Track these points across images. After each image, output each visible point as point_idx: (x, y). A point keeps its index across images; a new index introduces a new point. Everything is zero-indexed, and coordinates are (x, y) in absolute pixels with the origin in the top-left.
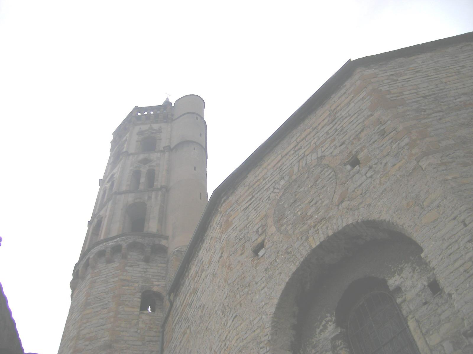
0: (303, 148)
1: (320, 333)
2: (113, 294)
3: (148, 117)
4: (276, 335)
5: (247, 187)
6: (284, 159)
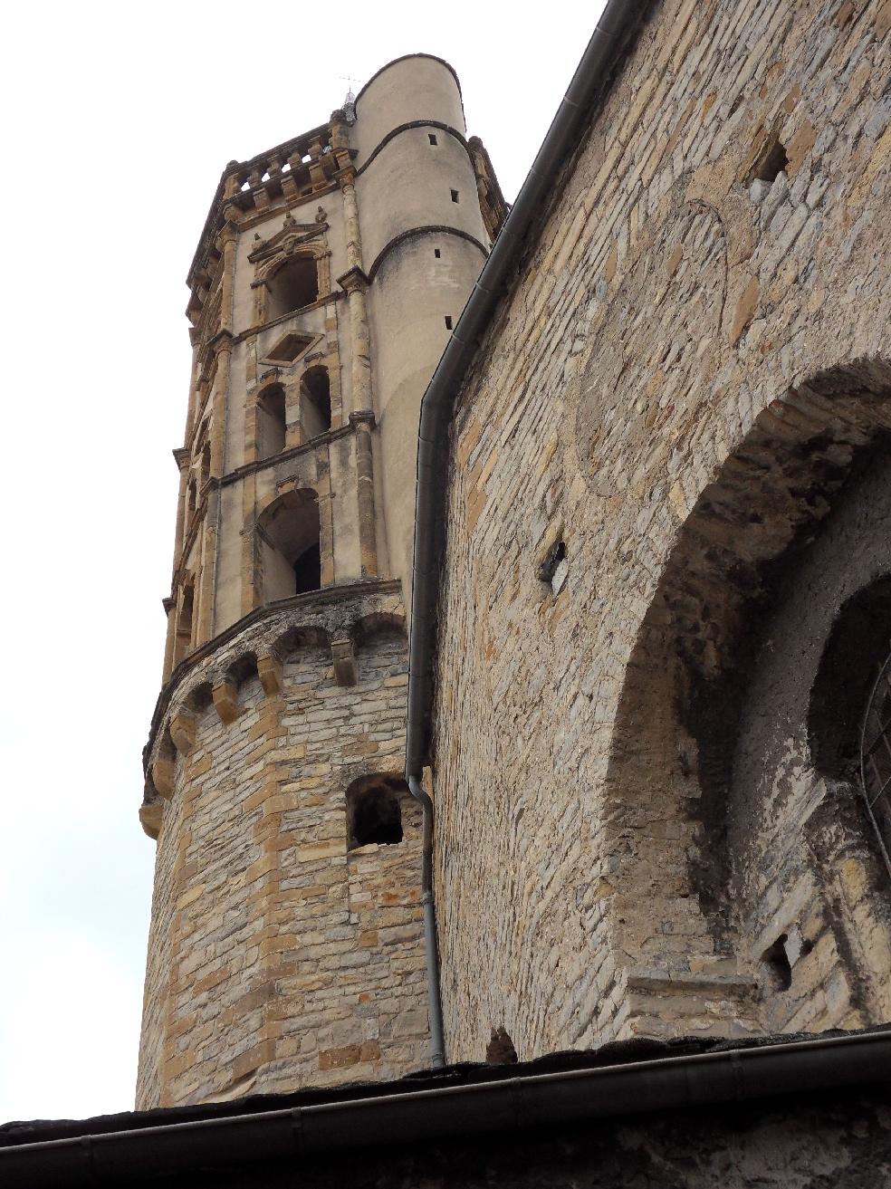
0: (636, 160)
1: (775, 816)
2: (255, 819)
3: (275, 191)
4: (628, 849)
5: (512, 356)
6: (593, 219)
